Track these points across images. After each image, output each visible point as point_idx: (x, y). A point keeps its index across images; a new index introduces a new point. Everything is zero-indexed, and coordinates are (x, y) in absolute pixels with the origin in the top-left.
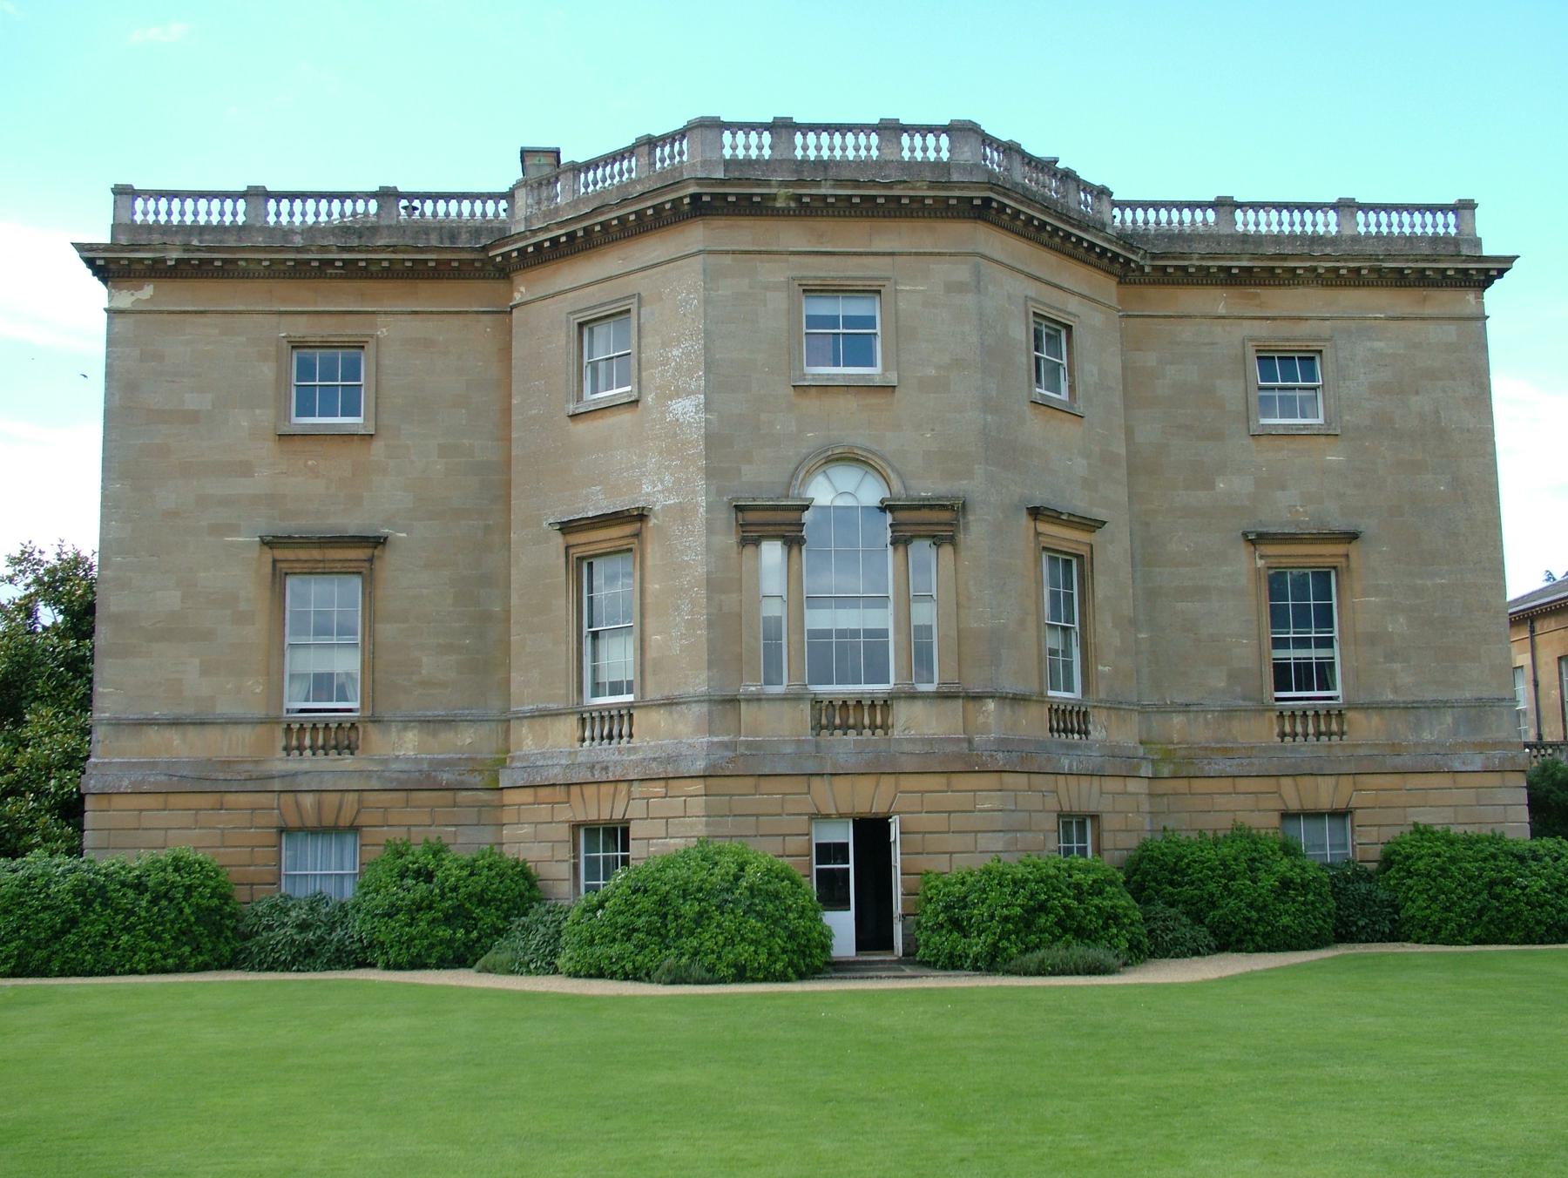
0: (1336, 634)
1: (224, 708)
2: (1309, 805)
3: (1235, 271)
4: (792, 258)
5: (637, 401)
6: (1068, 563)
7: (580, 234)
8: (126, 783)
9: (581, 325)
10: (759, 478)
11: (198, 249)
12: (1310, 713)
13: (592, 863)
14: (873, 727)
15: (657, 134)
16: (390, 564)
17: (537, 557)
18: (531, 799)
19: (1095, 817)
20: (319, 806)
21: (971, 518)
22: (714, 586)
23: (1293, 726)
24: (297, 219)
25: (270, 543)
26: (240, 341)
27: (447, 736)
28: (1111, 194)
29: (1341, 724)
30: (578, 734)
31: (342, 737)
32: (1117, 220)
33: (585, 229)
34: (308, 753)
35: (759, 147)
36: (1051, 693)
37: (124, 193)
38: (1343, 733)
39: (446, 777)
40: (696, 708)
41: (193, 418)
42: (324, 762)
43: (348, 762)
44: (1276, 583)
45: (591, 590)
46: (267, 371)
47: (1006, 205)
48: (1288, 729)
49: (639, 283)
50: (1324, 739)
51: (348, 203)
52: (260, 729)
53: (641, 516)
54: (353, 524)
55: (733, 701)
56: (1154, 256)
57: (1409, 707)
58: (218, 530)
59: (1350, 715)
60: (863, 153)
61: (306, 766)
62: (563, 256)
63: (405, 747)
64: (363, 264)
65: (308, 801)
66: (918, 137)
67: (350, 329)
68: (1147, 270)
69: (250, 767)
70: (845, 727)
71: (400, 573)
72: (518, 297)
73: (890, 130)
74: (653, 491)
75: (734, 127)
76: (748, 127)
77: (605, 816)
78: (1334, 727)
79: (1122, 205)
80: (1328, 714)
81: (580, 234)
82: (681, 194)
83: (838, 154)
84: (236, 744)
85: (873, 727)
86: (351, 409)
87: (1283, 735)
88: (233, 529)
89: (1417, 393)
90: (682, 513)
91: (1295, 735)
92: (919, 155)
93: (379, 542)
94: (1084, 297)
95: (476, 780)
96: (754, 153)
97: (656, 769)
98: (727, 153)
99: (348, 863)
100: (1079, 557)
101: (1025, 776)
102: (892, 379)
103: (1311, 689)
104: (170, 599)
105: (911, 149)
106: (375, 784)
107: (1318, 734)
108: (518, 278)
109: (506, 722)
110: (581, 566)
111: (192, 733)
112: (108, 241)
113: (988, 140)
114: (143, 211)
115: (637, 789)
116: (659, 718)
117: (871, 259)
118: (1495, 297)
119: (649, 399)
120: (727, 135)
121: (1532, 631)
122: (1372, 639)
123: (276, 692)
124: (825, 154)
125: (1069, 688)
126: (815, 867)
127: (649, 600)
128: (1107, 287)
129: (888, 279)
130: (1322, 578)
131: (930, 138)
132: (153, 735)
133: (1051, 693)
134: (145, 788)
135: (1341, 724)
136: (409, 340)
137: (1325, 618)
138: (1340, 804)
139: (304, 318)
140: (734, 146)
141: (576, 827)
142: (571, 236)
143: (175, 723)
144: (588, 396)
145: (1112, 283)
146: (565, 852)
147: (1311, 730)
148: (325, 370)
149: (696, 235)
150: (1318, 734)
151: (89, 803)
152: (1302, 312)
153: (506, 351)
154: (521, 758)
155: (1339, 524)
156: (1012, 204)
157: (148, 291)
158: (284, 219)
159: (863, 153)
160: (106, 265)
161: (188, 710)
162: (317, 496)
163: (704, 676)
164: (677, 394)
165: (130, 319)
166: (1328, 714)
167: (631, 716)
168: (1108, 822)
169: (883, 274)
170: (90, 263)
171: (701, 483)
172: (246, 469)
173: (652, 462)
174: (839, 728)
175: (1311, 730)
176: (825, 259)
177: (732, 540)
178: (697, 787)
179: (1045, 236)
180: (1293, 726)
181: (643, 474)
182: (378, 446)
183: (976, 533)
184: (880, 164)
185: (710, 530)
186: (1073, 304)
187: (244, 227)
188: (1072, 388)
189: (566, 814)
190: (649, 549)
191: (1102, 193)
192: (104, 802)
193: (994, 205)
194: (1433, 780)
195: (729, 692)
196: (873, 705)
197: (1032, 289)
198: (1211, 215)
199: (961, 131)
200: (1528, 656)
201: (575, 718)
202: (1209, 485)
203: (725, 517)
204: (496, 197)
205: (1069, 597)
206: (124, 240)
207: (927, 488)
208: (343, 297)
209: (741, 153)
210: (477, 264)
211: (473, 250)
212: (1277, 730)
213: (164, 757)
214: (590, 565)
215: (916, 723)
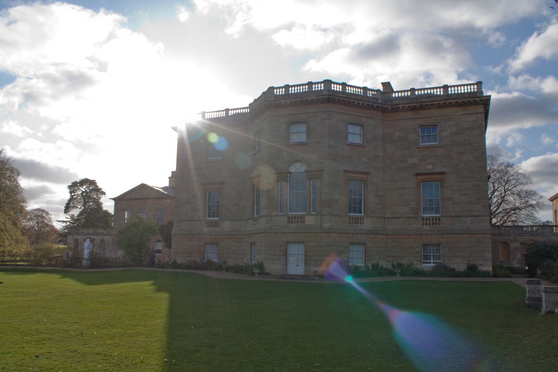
75: (277, 88)
78: (438, 222)
87: (423, 224)
103: (356, 213)
105: (315, 88)
107: (433, 224)
150: (433, 224)
212: (422, 223)
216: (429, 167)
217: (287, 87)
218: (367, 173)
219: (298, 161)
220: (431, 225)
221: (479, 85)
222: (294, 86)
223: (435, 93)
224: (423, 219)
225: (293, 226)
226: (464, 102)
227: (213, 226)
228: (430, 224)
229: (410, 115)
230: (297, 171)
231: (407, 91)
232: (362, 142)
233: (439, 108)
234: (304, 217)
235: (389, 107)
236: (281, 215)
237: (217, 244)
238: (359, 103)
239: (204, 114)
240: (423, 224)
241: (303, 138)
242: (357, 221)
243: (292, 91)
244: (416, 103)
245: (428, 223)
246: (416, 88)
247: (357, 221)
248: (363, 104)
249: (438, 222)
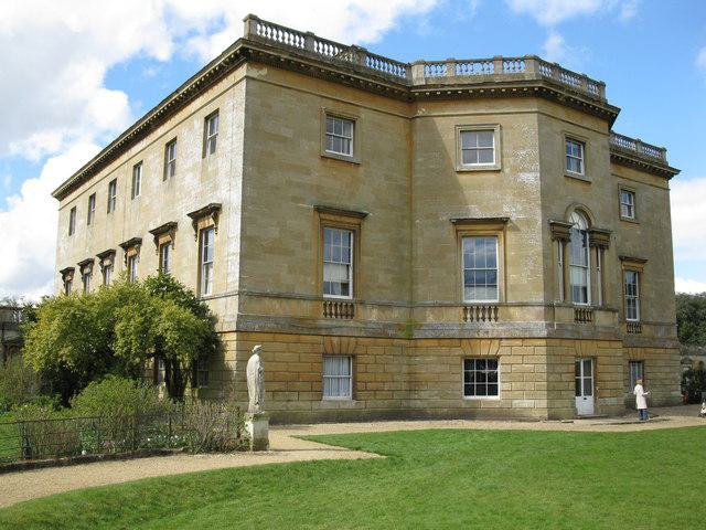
1: (299, 291)
5: (499, 171)
16: (367, 226)
19: (595, 358)
25: (318, 209)
26: (305, 104)
27: (388, 312)
30: (463, 316)
31: (348, 311)
34: (487, 320)
36: (325, 296)
39: (391, 332)
40: (537, 308)
41: (284, 140)
42: (342, 322)
43: (351, 323)
48: (350, 309)
49: (497, 119)
52: (315, 303)
54: (352, 205)
57: (655, 325)
58: (296, 199)
59: (644, 326)
61: (335, 323)
62: (392, 98)
63: (373, 316)
65: (335, 340)
67: (350, 112)
69: (311, 322)
71: (372, 235)
72: (420, 113)
84: (303, 309)
88: (303, 200)
90: (528, 223)
91: (331, 314)
93: (363, 216)
95: (401, 334)
104: (275, 232)
106: (363, 334)
109: (412, 306)
111: (284, 302)
114: (260, 30)
115: (504, 342)
116: (515, 312)
118: (673, 183)
119: (507, 170)
127: (508, 259)
132: (267, 301)
133: (325, 296)
134: (266, 330)
139: (331, 102)
143: (278, 297)
149: (534, 105)
153: (410, 136)
154: (426, 325)
155: (640, 256)
157: (264, 72)
161: (283, 290)
162: (337, 188)
163: (542, 294)
164: (524, 170)
165: (256, 84)
168: (600, 360)
171: (539, 211)
172: (308, 172)
173: (509, 198)
178: (543, 342)
182: (361, 169)
186: (584, 133)
189: (459, 352)
194: (658, 351)
196: (336, 305)
203: (547, 226)
208: (348, 96)
213: (272, 314)
232: (582, 173)
245: (481, 316)
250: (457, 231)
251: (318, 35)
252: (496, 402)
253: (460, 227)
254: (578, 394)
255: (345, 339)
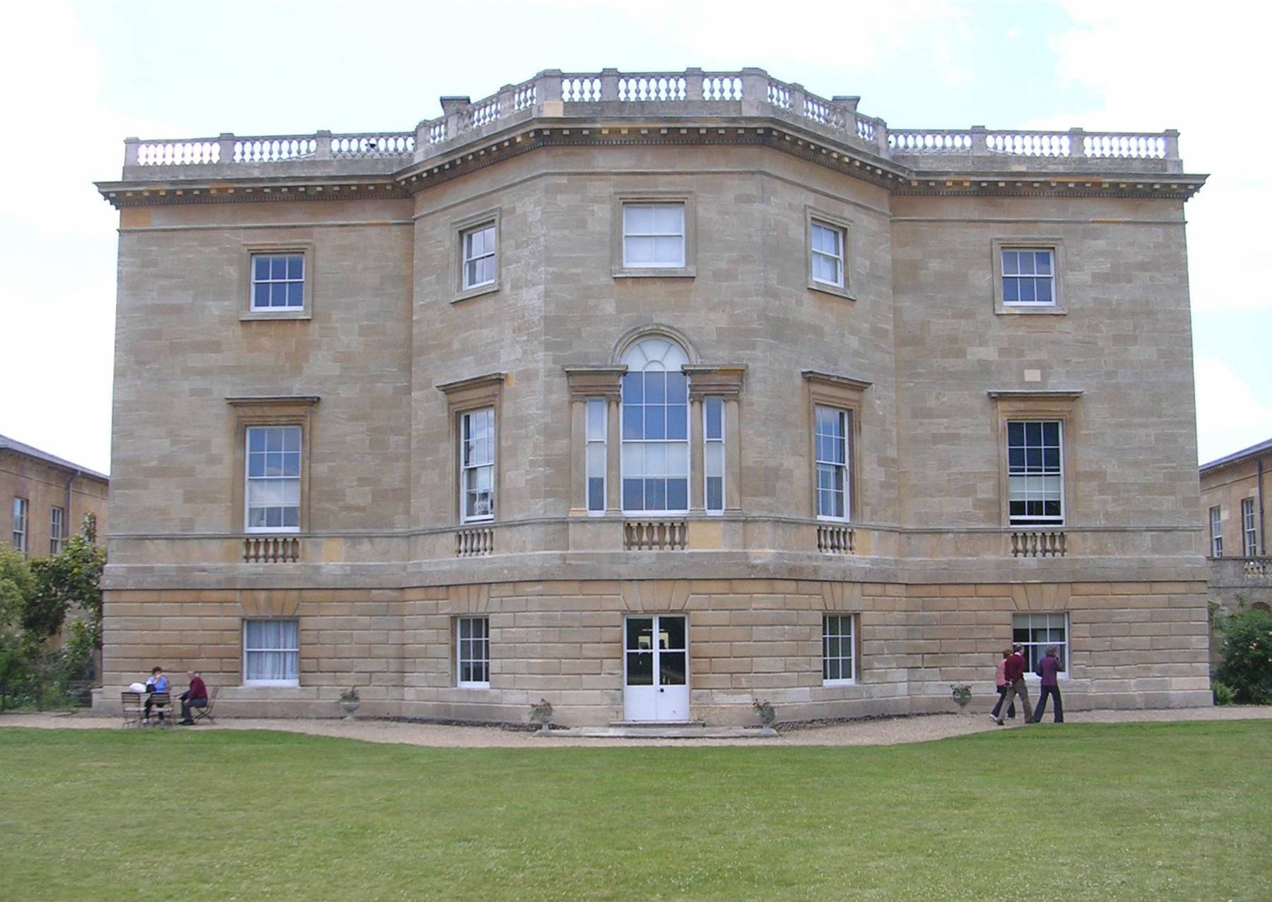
0: (1061, 472)
2: (1034, 607)
3: (984, 184)
4: (613, 177)
6: (842, 415)
7: (459, 162)
8: (131, 582)
9: (461, 233)
10: (593, 350)
11: (182, 182)
12: (1039, 534)
13: (465, 645)
14: (673, 543)
15: (515, 83)
17: (429, 409)
18: (422, 596)
19: (857, 615)
20: (269, 602)
21: (751, 380)
22: (550, 433)
23: (1025, 545)
24: (257, 157)
28: (885, 125)
29: (1062, 543)
30: (456, 547)
32: (892, 145)
33: (461, 158)
34: (262, 560)
35: (591, 92)
37: (133, 143)
38: (1064, 551)
44: (1015, 429)
45: (468, 436)
46: (233, 272)
47: (798, 139)
48: (1020, 546)
50: (1049, 555)
51: (304, 143)
53: (499, 380)
55: (564, 522)
56: (918, 173)
60: (673, 95)
64: (302, 189)
66: (716, 81)
67: (295, 241)
68: (915, 184)
70: (651, 544)
71: (333, 428)
73: (695, 75)
74: (507, 361)
75: (572, 77)
76: (582, 77)
77: (473, 610)
78: (1058, 546)
79: (897, 133)
80: (1053, 536)
81: (459, 162)
82: (528, 129)
83: (653, 96)
85: (673, 543)
86: (296, 301)
87: (1016, 552)
89: (1130, 281)
92: (717, 96)
94: (856, 204)
96: (587, 97)
97: (506, 575)
98: (566, 97)
99: (290, 642)
100: (850, 411)
101: (794, 583)
102: (692, 271)
103: (279, 525)
105: (710, 90)
107: (1045, 551)
108: (420, 197)
110: (460, 419)
112: (120, 179)
113: (773, 82)
114: (146, 156)
117: (677, 178)
120: (566, 83)
121: (1261, 470)
122: (1091, 476)
123: (238, 518)
124: (643, 96)
125: (840, 513)
126: (626, 651)
128: (882, 201)
129: (690, 193)
130: (1052, 429)
131: (727, 82)
133: (820, 517)
135: (1062, 543)
136: (344, 250)
137: (1053, 459)
138: (1058, 607)
140: (572, 91)
141: (454, 618)
142: (452, 163)
144: (466, 286)
145: (885, 195)
146: (445, 635)
147: (1039, 547)
148: (279, 274)
150: (1045, 551)
151: (106, 597)
152: (1044, 219)
153: (409, 256)
156: (790, 133)
158: (247, 157)
159: (673, 95)
160: (114, 194)
166: (1053, 536)
167: (492, 533)
168: (866, 618)
169: (686, 189)
170: (106, 196)
172: (216, 347)
174: (647, 543)
175: (1039, 547)
176: (640, 177)
177: (566, 398)
179: (822, 158)
180: (1025, 545)
181: (501, 347)
182: (314, 329)
183: (758, 393)
184: (687, 103)
185: (549, 390)
186: (848, 211)
187: (219, 165)
188: (846, 279)
189: (447, 608)
190: (505, 405)
191: (877, 123)
192: (115, 596)
193: (775, 133)
195: (560, 515)
197: (810, 200)
198: (968, 141)
199: (752, 75)
200: (1257, 489)
201: (453, 535)
202: (962, 353)
203: (561, 383)
204: (406, 135)
205: (842, 441)
206: (130, 178)
207: (721, 357)
209: (576, 97)
210: (389, 187)
211: (385, 176)
212: (1012, 548)
214: (467, 418)
215: (708, 541)
216: (1033, 375)
217: (610, 76)
218: (861, 387)
219: (657, 334)
220: (1039, 555)
221: (1076, 139)
222: (637, 76)
223: (1009, 149)
224: (248, 544)
225: (647, 555)
226: (1117, 184)
227: (275, 557)
228: (1034, 552)
229: (972, 209)
230: (649, 369)
231: (962, 133)
232: (840, 284)
233: (1060, 195)
234: (683, 526)
235: (913, 177)
236: (601, 521)
237: (294, 621)
238: (841, 157)
239: (133, 143)
240: (1016, 552)
241: (672, 259)
242: (838, 538)
243: (629, 91)
244: (998, 174)
245: (1029, 546)
246: (989, 128)
247: (838, 538)
248: (841, 157)
249: (1058, 546)
250: (450, 404)
251: (809, 88)
252: (482, 692)
253: (816, 388)
254: (825, 678)
255: (279, 595)
